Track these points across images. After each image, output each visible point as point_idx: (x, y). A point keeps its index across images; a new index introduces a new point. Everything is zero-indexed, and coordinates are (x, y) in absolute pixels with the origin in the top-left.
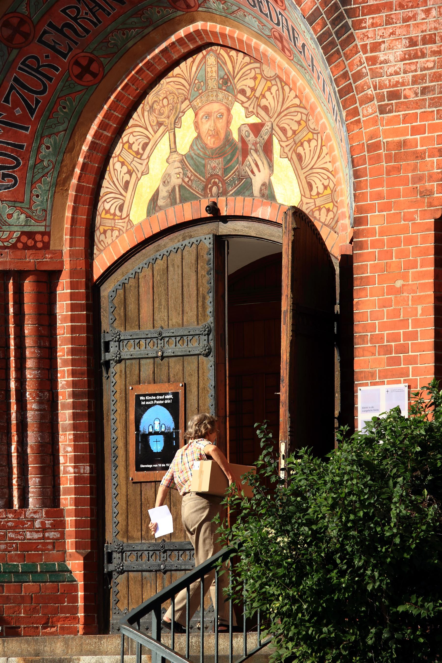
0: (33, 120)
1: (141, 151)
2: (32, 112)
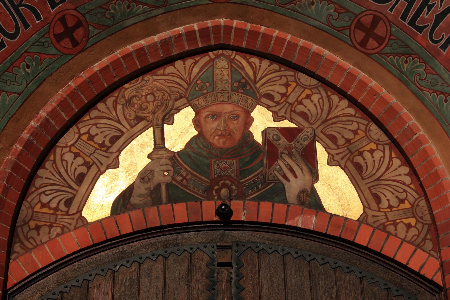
1: (107, 143)
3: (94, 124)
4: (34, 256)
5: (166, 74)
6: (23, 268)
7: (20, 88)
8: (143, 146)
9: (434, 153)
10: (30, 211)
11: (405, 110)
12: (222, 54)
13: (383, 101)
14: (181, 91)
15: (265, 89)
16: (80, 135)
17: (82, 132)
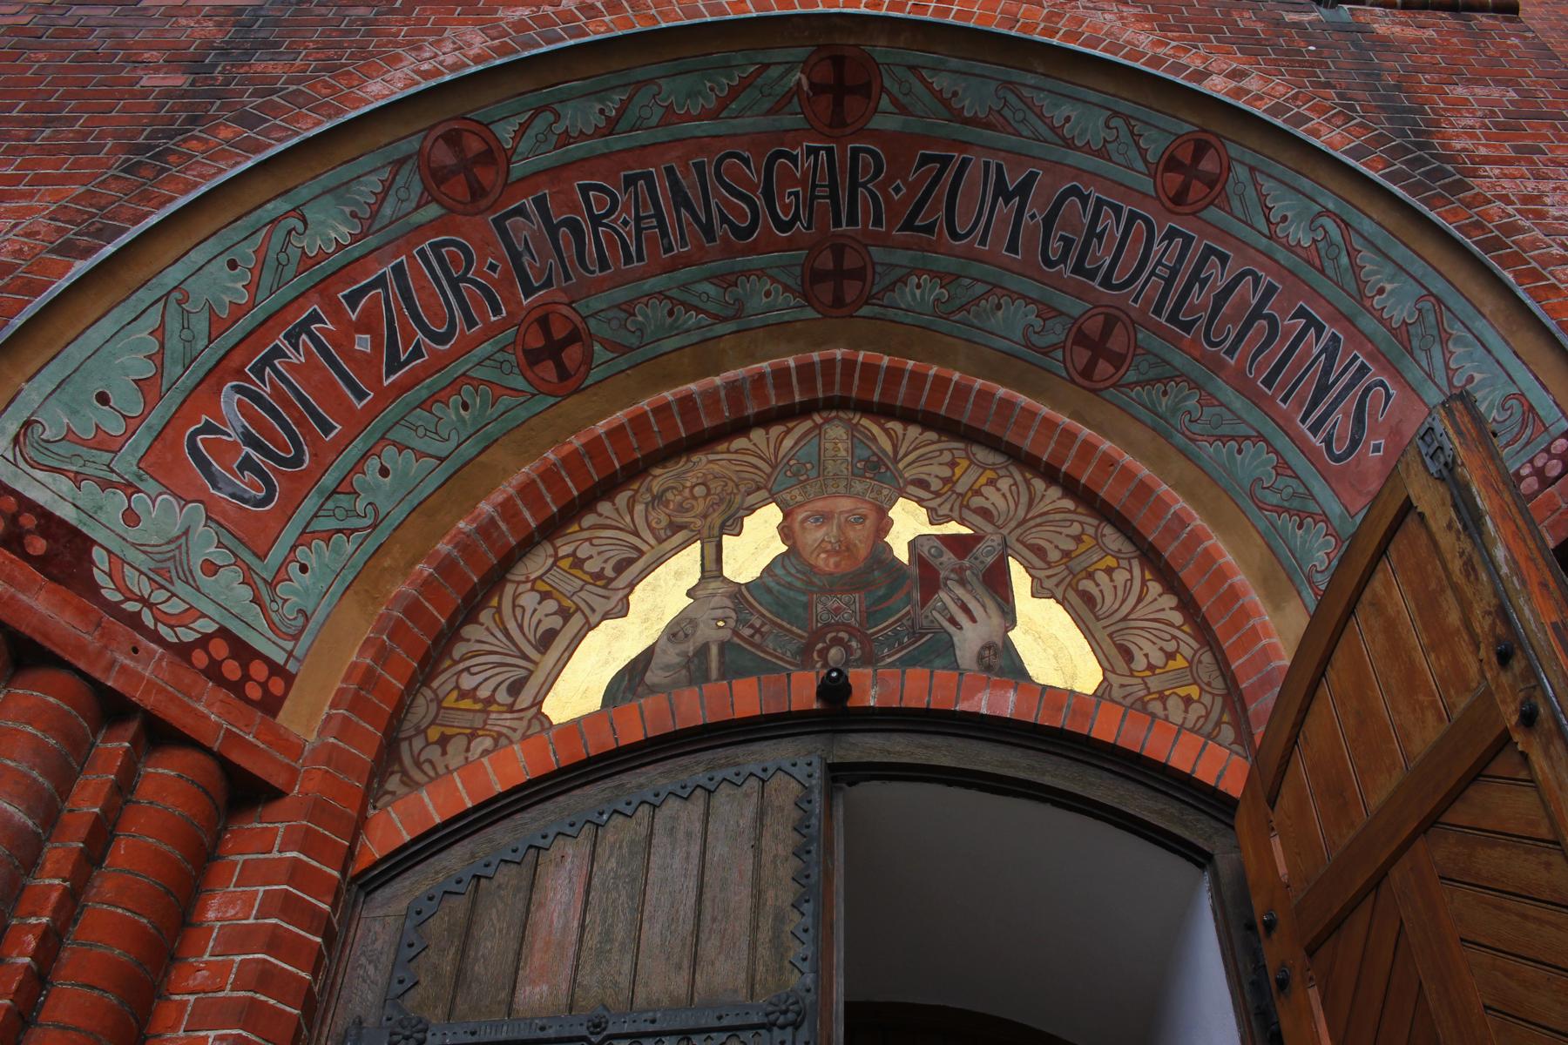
0: (386, 383)
1: (609, 572)
3: (586, 540)
4: (427, 800)
5: (732, 450)
6: (399, 825)
7: (443, 449)
8: (678, 575)
9: (1223, 556)
10: (433, 706)
11: (1165, 487)
13: (1127, 474)
14: (758, 479)
15: (914, 471)
16: (557, 559)
17: (561, 554)
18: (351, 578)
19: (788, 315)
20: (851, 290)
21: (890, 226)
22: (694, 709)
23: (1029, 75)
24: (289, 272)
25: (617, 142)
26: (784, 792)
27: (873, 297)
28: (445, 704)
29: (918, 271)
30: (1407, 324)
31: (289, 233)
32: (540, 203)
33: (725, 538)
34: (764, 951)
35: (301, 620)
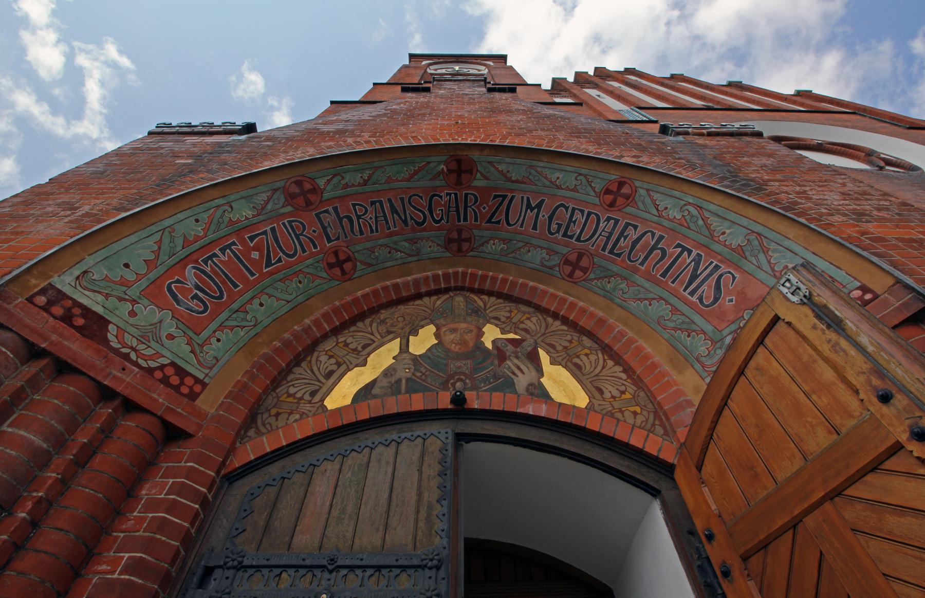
0: (265, 271)
1: (360, 348)
2: (269, 264)
3: (351, 336)
7: (289, 298)
10: (275, 400)
12: (460, 294)
13: (592, 315)
16: (337, 343)
17: (339, 341)
18: (242, 345)
19: (438, 255)
20: (465, 246)
21: (481, 222)
22: (393, 406)
23: (540, 163)
24: (223, 226)
25: (368, 188)
26: (434, 445)
27: (475, 249)
28: (280, 399)
29: (492, 238)
30: (741, 246)
31: (224, 211)
32: (335, 209)
33: (411, 337)
34: (422, 524)
35: (214, 361)
